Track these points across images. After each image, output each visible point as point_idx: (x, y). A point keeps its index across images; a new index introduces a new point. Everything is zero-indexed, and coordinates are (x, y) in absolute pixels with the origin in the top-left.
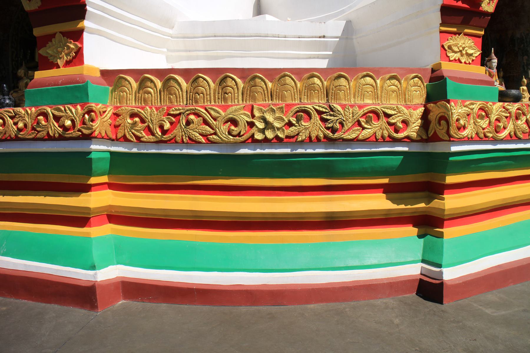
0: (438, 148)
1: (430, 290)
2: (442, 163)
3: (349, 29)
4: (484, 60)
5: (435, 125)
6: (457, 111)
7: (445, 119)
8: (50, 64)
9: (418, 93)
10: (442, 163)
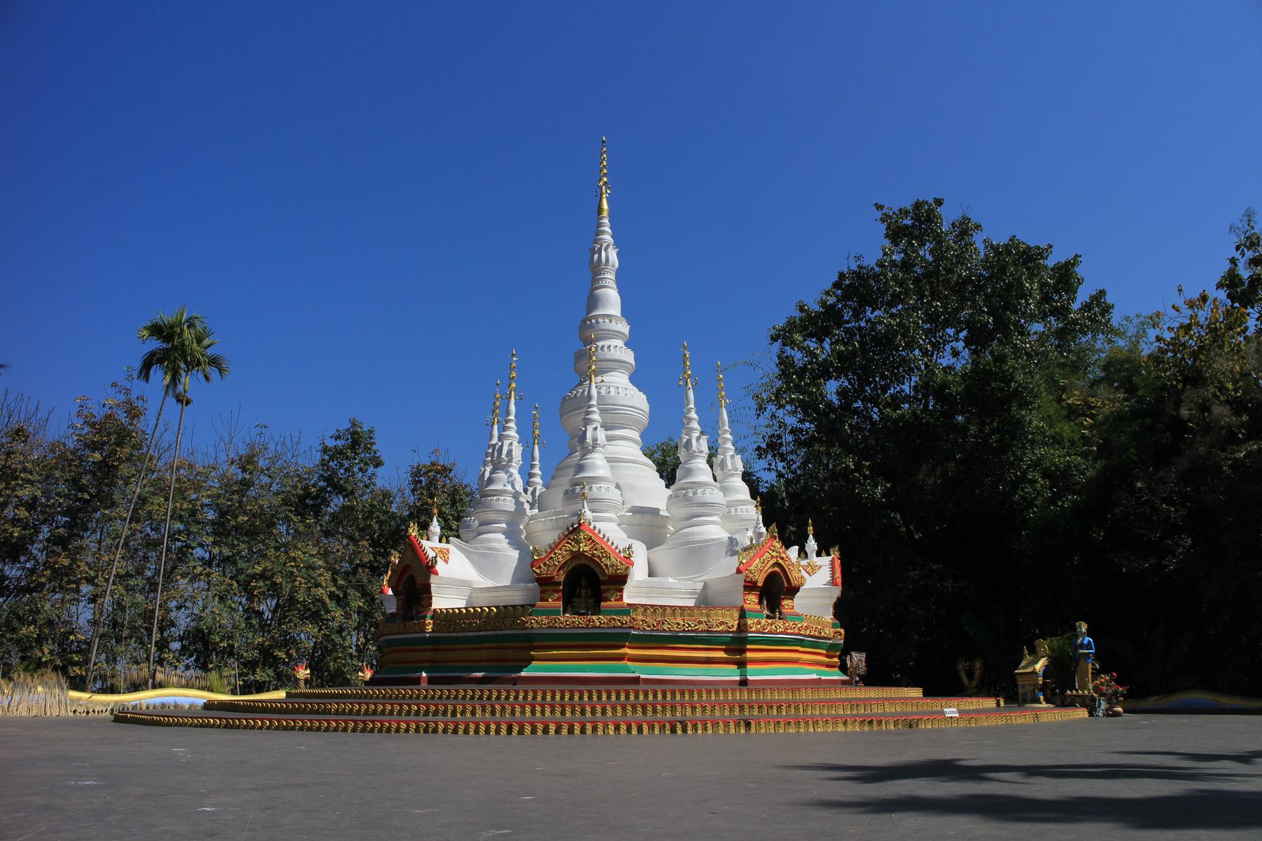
0: (743, 635)
1: (744, 682)
2: (745, 641)
3: (705, 586)
4: (760, 603)
5: (742, 627)
6: (749, 622)
7: (746, 624)
8: (607, 600)
9: (736, 615)
10: (745, 641)
